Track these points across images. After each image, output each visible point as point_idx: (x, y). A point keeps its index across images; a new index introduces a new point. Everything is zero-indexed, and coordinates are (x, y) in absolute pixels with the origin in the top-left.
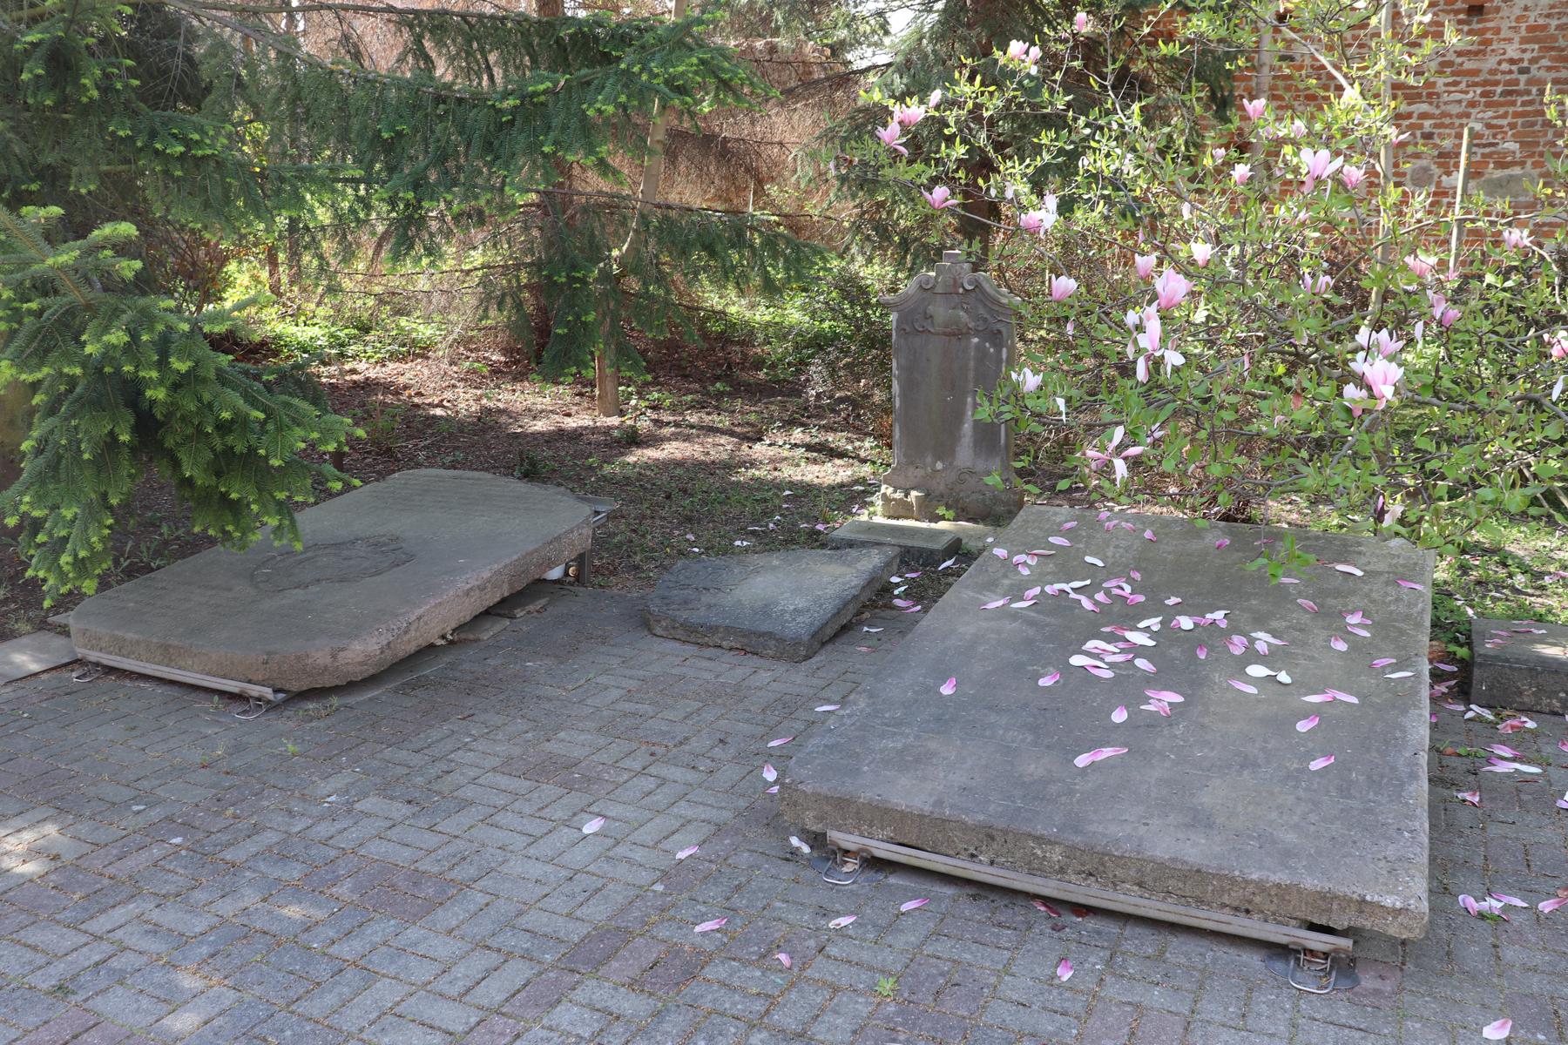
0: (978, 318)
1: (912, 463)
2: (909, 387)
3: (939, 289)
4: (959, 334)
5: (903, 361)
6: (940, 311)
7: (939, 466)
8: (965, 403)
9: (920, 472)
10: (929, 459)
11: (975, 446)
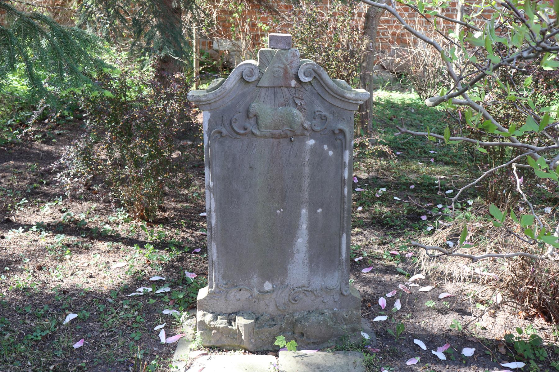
0: (313, 116)
1: (234, 286)
2: (228, 198)
3: (265, 82)
4: (291, 135)
5: (217, 170)
6: (266, 108)
7: (268, 286)
8: (299, 215)
9: (244, 295)
10: (255, 280)
11: (311, 262)
